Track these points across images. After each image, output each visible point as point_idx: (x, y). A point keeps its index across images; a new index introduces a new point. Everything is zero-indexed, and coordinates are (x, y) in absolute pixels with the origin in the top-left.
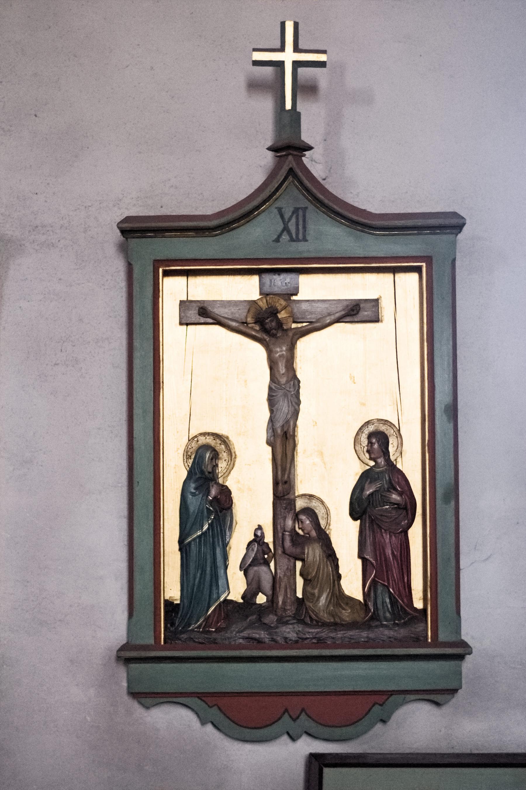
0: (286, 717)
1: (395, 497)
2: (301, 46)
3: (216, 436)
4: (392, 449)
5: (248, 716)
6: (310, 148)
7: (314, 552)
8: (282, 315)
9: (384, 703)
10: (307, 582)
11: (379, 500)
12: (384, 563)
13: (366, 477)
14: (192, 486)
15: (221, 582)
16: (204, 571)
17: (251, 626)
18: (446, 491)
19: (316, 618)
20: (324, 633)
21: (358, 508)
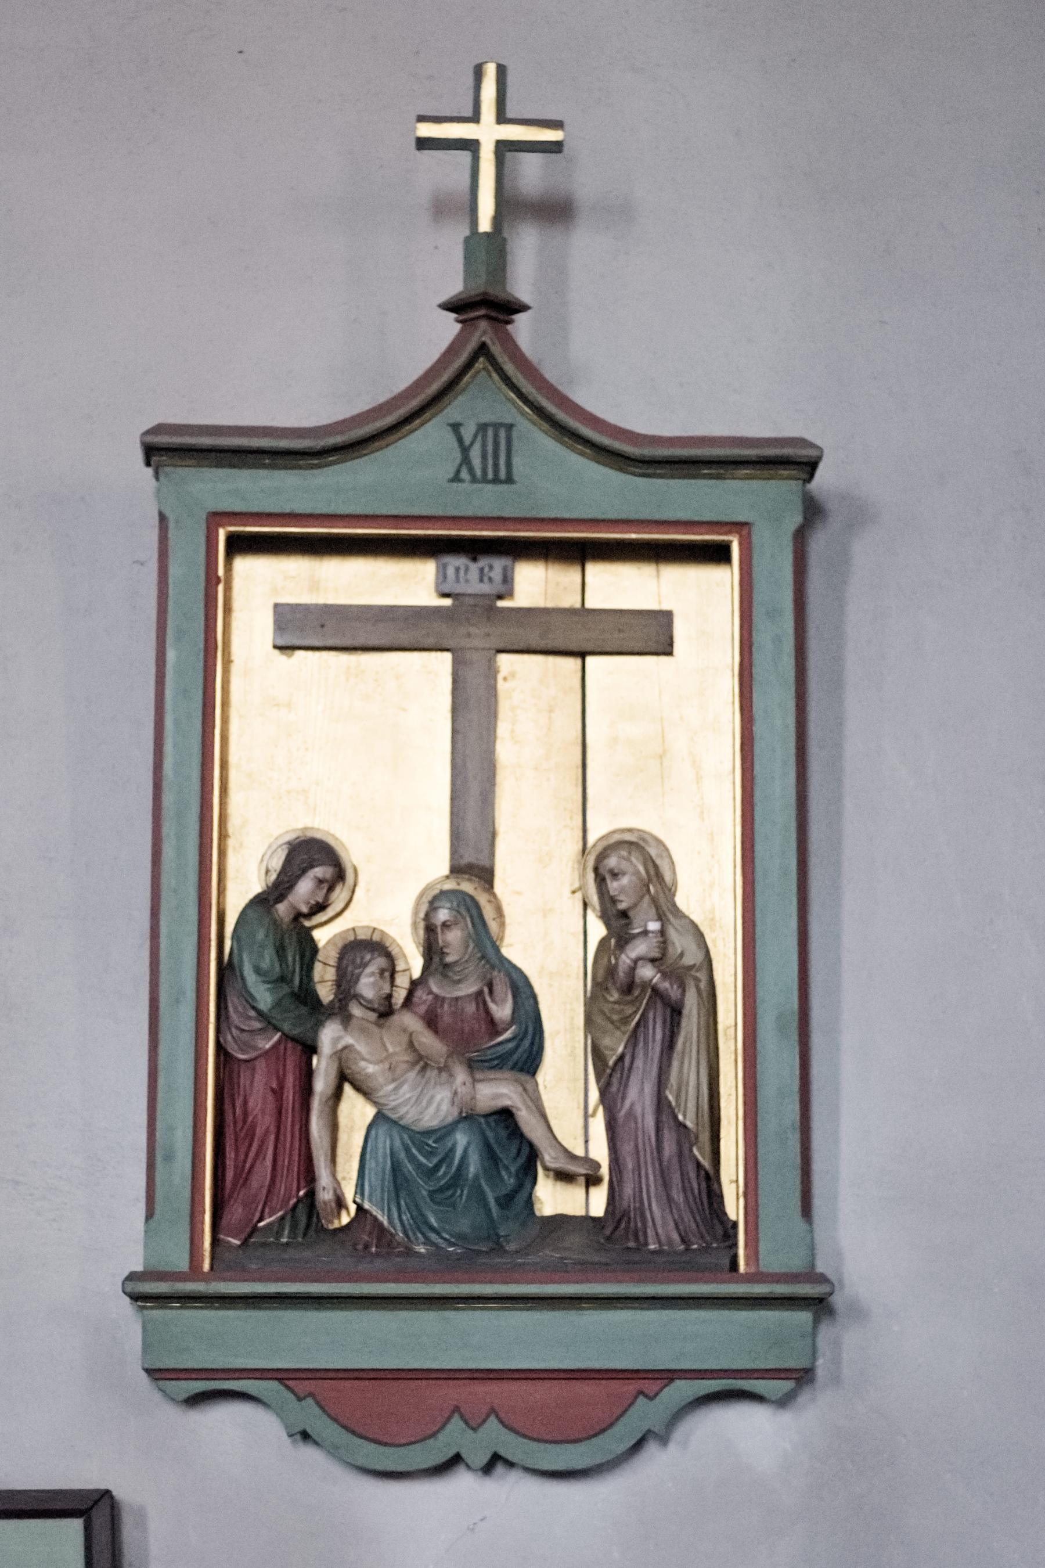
0: (456, 1422)
2: (510, 114)
6: (522, 308)
9: (657, 1394)
11: (646, 996)
19: (226, 1196)
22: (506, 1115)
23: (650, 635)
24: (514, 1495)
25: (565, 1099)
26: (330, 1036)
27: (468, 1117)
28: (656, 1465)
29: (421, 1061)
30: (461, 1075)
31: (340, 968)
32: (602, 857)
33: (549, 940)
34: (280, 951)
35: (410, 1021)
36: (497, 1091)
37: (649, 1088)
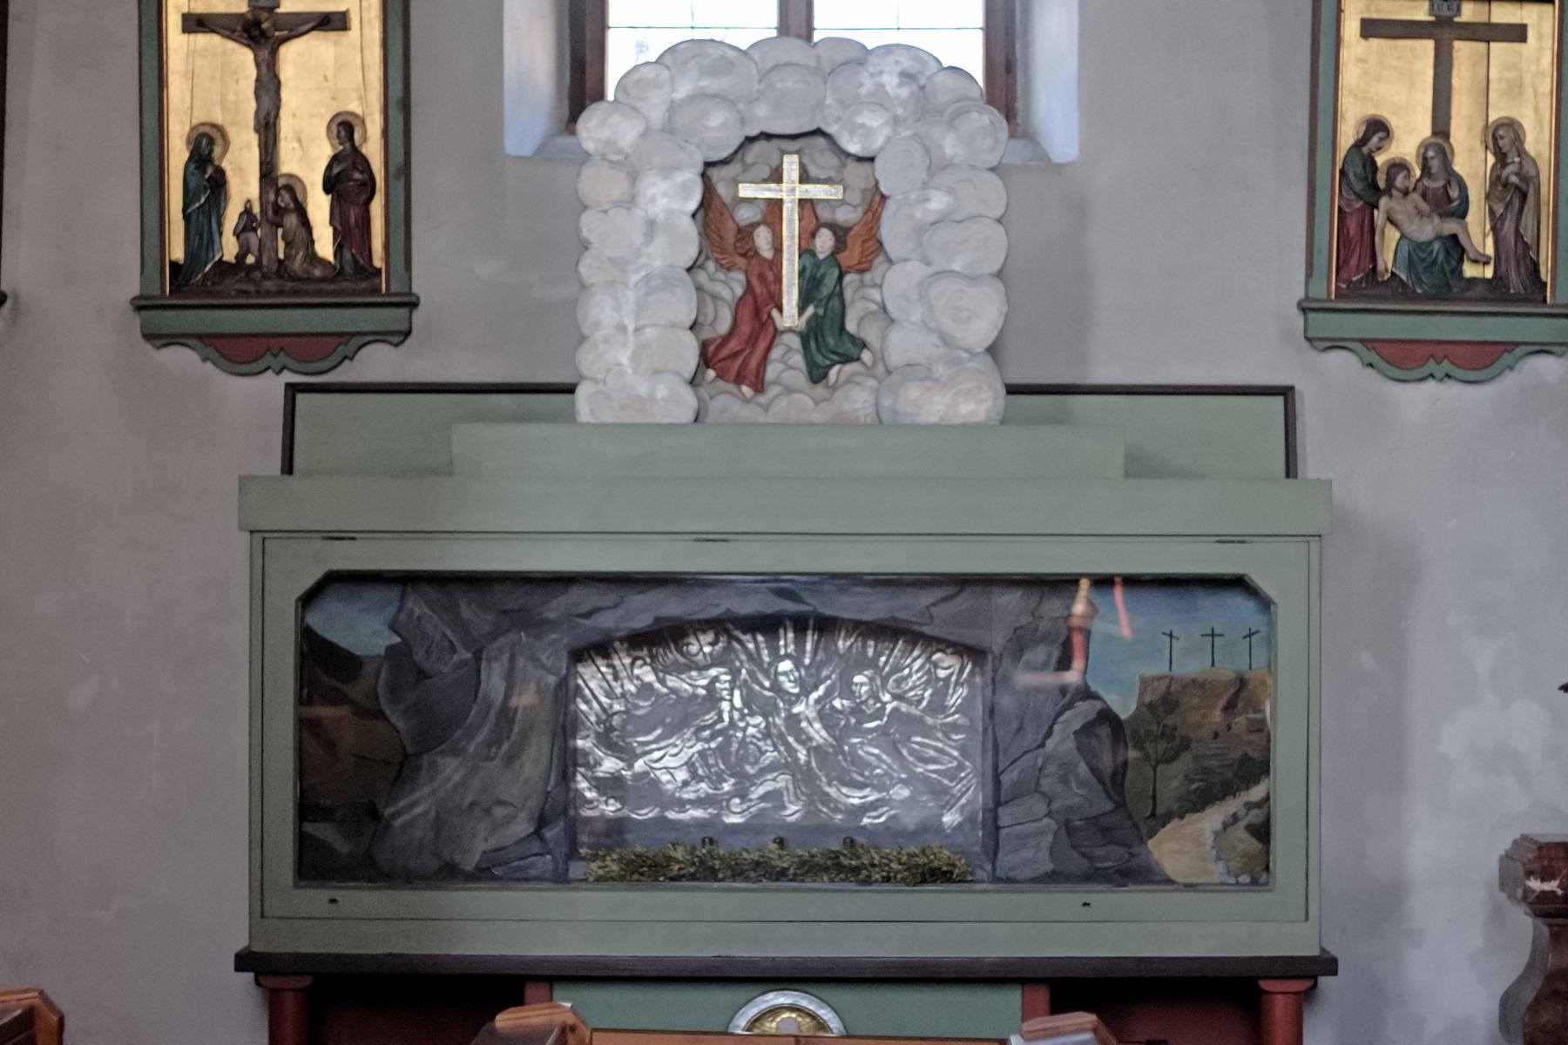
1: (357, 176)
3: (214, 126)
4: (357, 136)
5: (238, 353)
7: (291, 220)
8: (265, 26)
10: (287, 245)
11: (347, 179)
12: (351, 231)
13: (335, 159)
14: (192, 167)
15: (217, 246)
16: (201, 239)
17: (240, 280)
18: (402, 171)
20: (300, 286)
21: (331, 184)
22: (1454, 237)
23: (1518, 33)
24: (1452, 390)
25: (1478, 231)
26: (1384, 202)
27: (1439, 237)
28: (1509, 381)
29: (1420, 213)
30: (1437, 219)
31: (1388, 174)
32: (1496, 130)
33: (1472, 163)
34: (1364, 166)
35: (1416, 197)
36: (1451, 227)
37: (1513, 225)
